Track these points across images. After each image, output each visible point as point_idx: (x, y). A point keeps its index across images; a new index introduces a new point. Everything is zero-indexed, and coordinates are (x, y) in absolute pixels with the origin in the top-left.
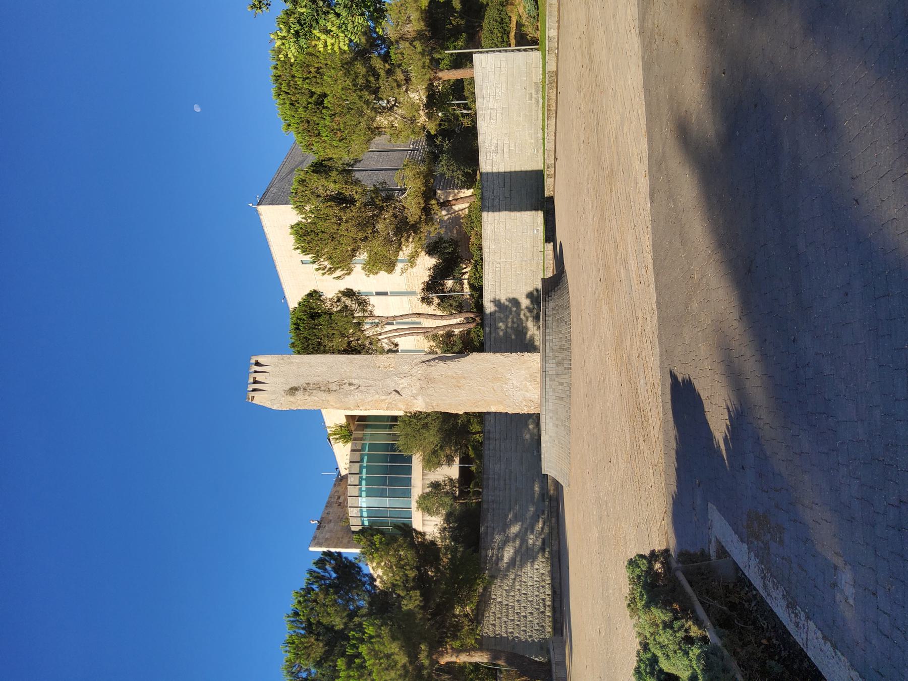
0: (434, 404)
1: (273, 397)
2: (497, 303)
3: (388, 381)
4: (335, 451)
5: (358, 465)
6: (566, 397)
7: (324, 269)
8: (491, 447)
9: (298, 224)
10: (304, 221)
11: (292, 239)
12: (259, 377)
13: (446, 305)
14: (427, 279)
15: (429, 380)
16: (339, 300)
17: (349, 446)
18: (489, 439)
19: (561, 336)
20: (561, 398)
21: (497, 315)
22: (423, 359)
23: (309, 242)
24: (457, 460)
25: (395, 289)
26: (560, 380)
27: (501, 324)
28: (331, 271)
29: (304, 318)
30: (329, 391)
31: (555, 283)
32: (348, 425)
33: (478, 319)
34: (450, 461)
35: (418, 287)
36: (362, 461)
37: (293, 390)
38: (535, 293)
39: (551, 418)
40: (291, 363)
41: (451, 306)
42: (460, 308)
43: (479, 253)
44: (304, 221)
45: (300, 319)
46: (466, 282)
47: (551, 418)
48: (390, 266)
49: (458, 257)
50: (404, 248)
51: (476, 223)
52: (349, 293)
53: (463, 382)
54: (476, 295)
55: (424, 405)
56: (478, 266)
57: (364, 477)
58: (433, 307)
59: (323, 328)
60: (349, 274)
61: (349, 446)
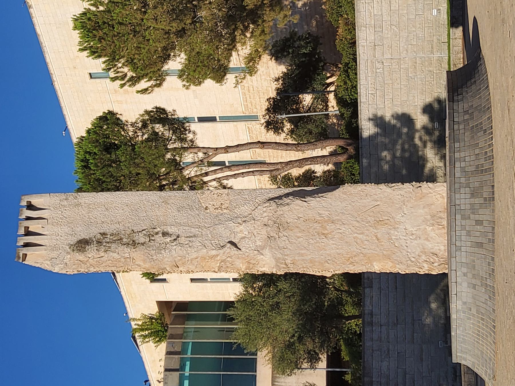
0: (288, 261)
1: (54, 254)
2: (378, 121)
3: (220, 229)
4: (143, 355)
5: (177, 374)
6: (487, 244)
7: (123, 78)
8: (375, 336)
9: (84, 14)
10: (93, 9)
11: (76, 36)
12: (33, 226)
13: (301, 132)
14: (273, 94)
15: (280, 225)
16: (145, 125)
17: (163, 346)
18: (371, 324)
19: (477, 151)
20: (480, 245)
21: (380, 139)
22: (271, 195)
23: (101, 39)
24: (324, 357)
25: (228, 105)
26: (477, 217)
27: (385, 153)
28: (134, 81)
29: (96, 151)
30: (134, 244)
31: (466, 78)
32: (162, 315)
33: (351, 150)
34: (313, 359)
35: (260, 107)
36: (182, 368)
37: (82, 245)
38: (436, 106)
39: (465, 275)
40: (79, 205)
41: (311, 133)
42: (324, 135)
43: (350, 51)
44: (93, 9)
45: (90, 153)
46: (331, 97)
47: (465, 275)
48: (220, 73)
49: (319, 60)
50: (239, 46)
51: (346, 7)
52: (160, 116)
53: (330, 227)
54: (347, 114)
55: (273, 263)
56: (350, 70)
57: (187, 374)
58: (283, 135)
59: (123, 158)
60: (159, 85)
61: (163, 346)
